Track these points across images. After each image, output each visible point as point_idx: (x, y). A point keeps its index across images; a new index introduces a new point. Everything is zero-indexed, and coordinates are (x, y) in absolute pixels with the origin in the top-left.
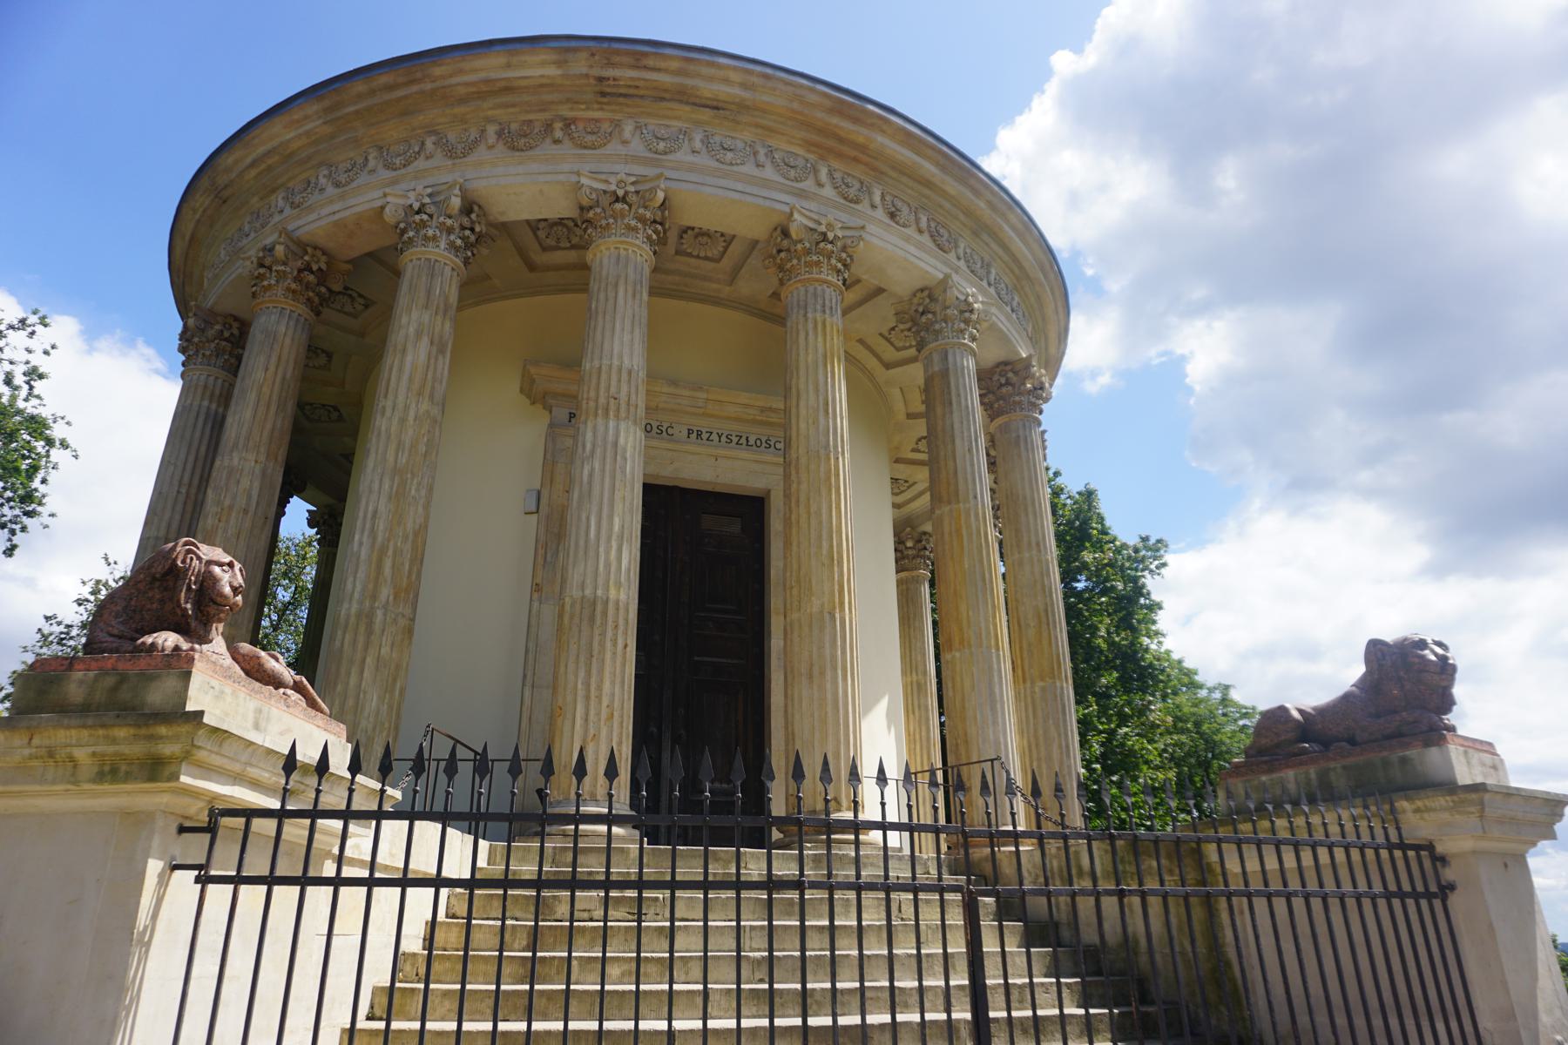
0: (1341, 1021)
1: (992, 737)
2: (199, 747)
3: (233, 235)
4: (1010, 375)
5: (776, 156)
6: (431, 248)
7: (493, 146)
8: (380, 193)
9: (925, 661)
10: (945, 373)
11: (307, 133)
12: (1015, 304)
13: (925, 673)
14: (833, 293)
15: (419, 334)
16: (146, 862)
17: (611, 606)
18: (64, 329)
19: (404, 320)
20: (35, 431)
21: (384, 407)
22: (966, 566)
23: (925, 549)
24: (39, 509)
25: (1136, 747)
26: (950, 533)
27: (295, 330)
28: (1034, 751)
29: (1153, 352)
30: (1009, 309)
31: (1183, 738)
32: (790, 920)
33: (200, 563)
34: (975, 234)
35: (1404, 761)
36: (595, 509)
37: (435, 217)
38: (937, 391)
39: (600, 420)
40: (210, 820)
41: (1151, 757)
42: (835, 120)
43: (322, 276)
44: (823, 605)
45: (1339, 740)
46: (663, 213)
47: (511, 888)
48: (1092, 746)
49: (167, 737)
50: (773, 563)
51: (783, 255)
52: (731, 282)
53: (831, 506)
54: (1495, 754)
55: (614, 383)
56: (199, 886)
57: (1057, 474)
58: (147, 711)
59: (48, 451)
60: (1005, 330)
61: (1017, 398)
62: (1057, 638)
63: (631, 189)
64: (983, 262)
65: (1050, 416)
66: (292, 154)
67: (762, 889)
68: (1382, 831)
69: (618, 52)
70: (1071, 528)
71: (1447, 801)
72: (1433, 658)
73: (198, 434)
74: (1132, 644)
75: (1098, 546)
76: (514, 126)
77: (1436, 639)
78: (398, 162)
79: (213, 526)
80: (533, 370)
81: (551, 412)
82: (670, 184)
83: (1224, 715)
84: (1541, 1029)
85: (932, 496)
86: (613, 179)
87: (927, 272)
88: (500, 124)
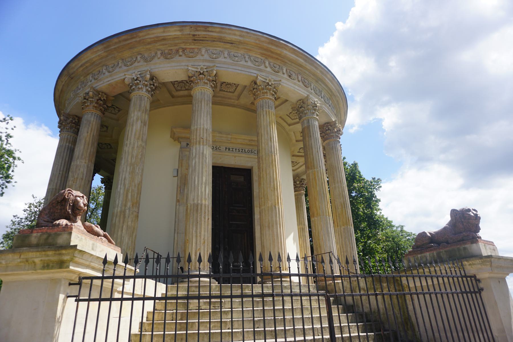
0: (449, 334)
2: (76, 257)
3: (75, 89)
4: (329, 127)
5: (252, 58)
6: (140, 91)
7: (160, 58)
8: (123, 74)
9: (304, 221)
10: (308, 127)
11: (99, 56)
12: (330, 104)
13: (304, 225)
14: (272, 102)
15: (137, 119)
17: (203, 206)
18: (18, 121)
19: (132, 115)
20: (9, 154)
21: (127, 144)
22: (318, 189)
23: (303, 184)
24: (11, 180)
25: (374, 247)
26: (312, 179)
27: (97, 119)
28: (342, 249)
29: (371, 119)
30: (328, 105)
31: (389, 243)
32: (279, 307)
33: (73, 196)
34: (317, 82)
35: (465, 249)
36: (197, 174)
37: (141, 82)
38: (306, 133)
39: (198, 146)
41: (379, 250)
42: (270, 46)
43: (105, 102)
45: (443, 242)
46: (216, 78)
48: (359, 247)
49: (65, 254)
50: (255, 190)
51: (255, 90)
55: (202, 133)
56: (76, 302)
57: (344, 158)
58: (58, 246)
59: (14, 161)
60: (327, 112)
61: (332, 134)
62: (348, 212)
64: (319, 90)
65: (343, 140)
66: (94, 62)
67: (260, 297)
69: (199, 26)
70: (350, 176)
71: (480, 261)
72: (473, 215)
73: (65, 154)
74: (371, 213)
75: (359, 181)
76: (166, 51)
77: (473, 208)
78: (129, 64)
80: (174, 130)
81: (181, 143)
83: (402, 235)
85: (306, 167)
86: (199, 67)
87: (302, 94)
88: (162, 51)
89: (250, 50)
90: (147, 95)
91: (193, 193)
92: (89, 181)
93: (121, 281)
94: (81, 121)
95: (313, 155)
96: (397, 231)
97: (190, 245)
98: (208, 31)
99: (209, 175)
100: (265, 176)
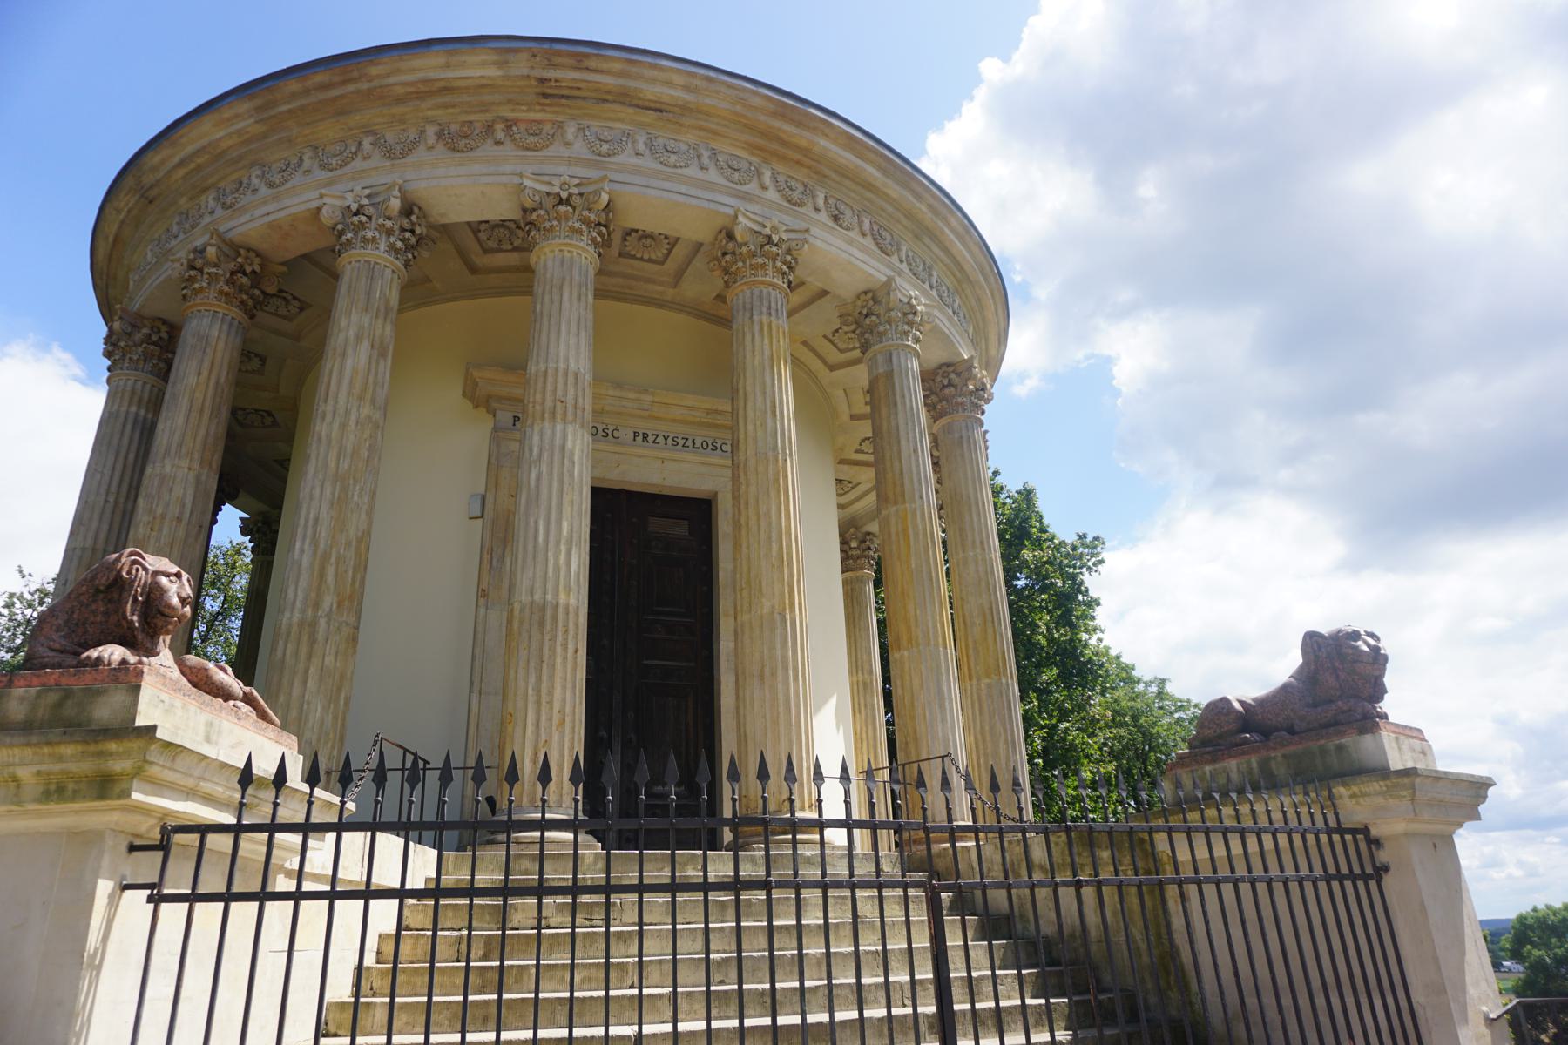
0: (1287, 1001)
1: (940, 734)
2: (152, 763)
4: (953, 376)
5: (720, 159)
6: (370, 250)
7: (433, 147)
8: (317, 194)
10: (889, 375)
11: (239, 132)
12: (956, 306)
13: (871, 672)
15: (359, 338)
16: (96, 883)
17: (561, 610)
19: (344, 323)
21: (324, 413)
22: (913, 566)
23: (869, 549)
26: (897, 534)
27: (229, 333)
28: (981, 747)
29: (1080, 355)
30: (950, 311)
33: (147, 573)
35: (1340, 748)
36: (543, 513)
38: (881, 392)
39: (547, 424)
40: (163, 837)
41: (1092, 751)
42: (777, 124)
44: (773, 606)
45: (1277, 730)
46: (607, 215)
47: (477, 896)
48: (1034, 741)
50: (721, 565)
51: (728, 257)
52: (675, 285)
53: (780, 508)
54: (1424, 740)
55: (560, 386)
57: (996, 473)
58: (94, 727)
60: (947, 331)
61: (960, 400)
63: (576, 191)
64: (924, 264)
65: (993, 416)
66: (223, 152)
68: (1321, 816)
69: (559, 54)
71: (1380, 786)
72: (1365, 648)
73: (126, 441)
74: (1072, 640)
75: (1038, 544)
76: (454, 127)
77: (1369, 631)
78: (334, 162)
79: (144, 535)
80: (476, 374)
82: (617, 187)
83: (1161, 708)
84: (1469, 1001)
85: (878, 496)
86: (557, 182)
87: (871, 275)
88: (440, 125)
89: (715, 133)
90: (392, 263)
91: (531, 569)
92: (201, 527)
93: (295, 839)
94: (179, 336)
95: (900, 462)
96: (1146, 694)
97: (519, 731)
98: (587, 69)
99: (580, 515)
100: (753, 522)
